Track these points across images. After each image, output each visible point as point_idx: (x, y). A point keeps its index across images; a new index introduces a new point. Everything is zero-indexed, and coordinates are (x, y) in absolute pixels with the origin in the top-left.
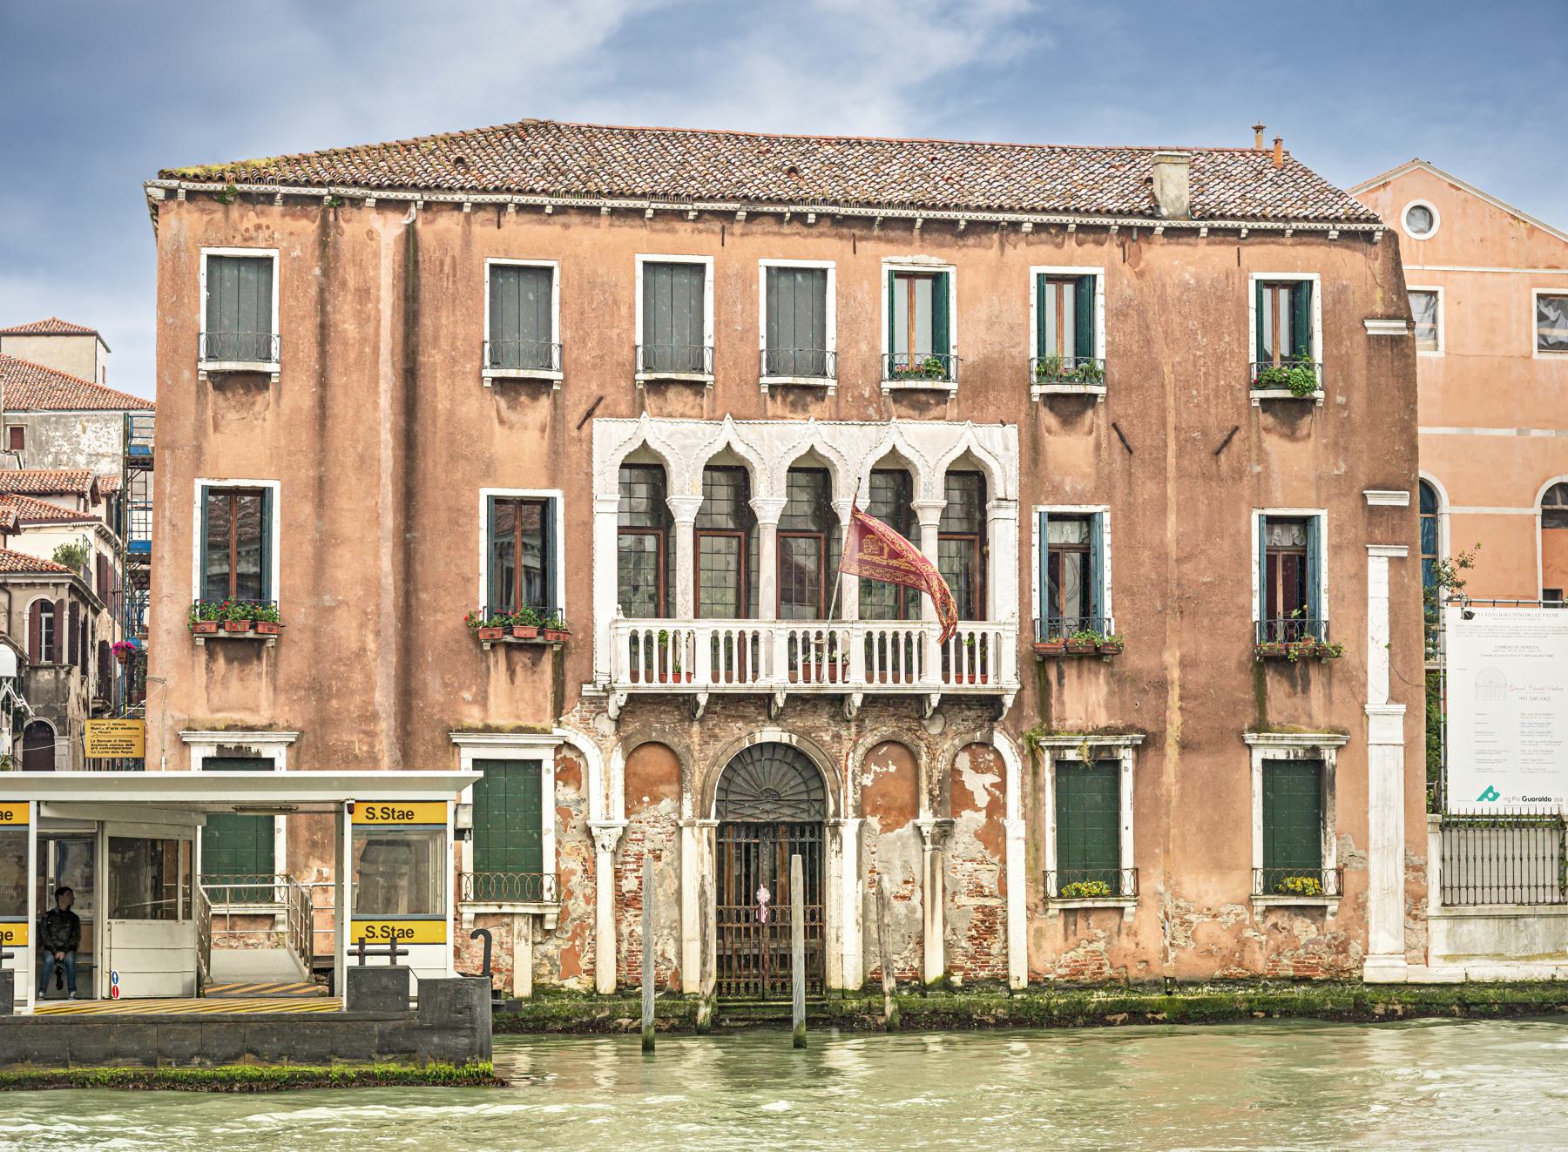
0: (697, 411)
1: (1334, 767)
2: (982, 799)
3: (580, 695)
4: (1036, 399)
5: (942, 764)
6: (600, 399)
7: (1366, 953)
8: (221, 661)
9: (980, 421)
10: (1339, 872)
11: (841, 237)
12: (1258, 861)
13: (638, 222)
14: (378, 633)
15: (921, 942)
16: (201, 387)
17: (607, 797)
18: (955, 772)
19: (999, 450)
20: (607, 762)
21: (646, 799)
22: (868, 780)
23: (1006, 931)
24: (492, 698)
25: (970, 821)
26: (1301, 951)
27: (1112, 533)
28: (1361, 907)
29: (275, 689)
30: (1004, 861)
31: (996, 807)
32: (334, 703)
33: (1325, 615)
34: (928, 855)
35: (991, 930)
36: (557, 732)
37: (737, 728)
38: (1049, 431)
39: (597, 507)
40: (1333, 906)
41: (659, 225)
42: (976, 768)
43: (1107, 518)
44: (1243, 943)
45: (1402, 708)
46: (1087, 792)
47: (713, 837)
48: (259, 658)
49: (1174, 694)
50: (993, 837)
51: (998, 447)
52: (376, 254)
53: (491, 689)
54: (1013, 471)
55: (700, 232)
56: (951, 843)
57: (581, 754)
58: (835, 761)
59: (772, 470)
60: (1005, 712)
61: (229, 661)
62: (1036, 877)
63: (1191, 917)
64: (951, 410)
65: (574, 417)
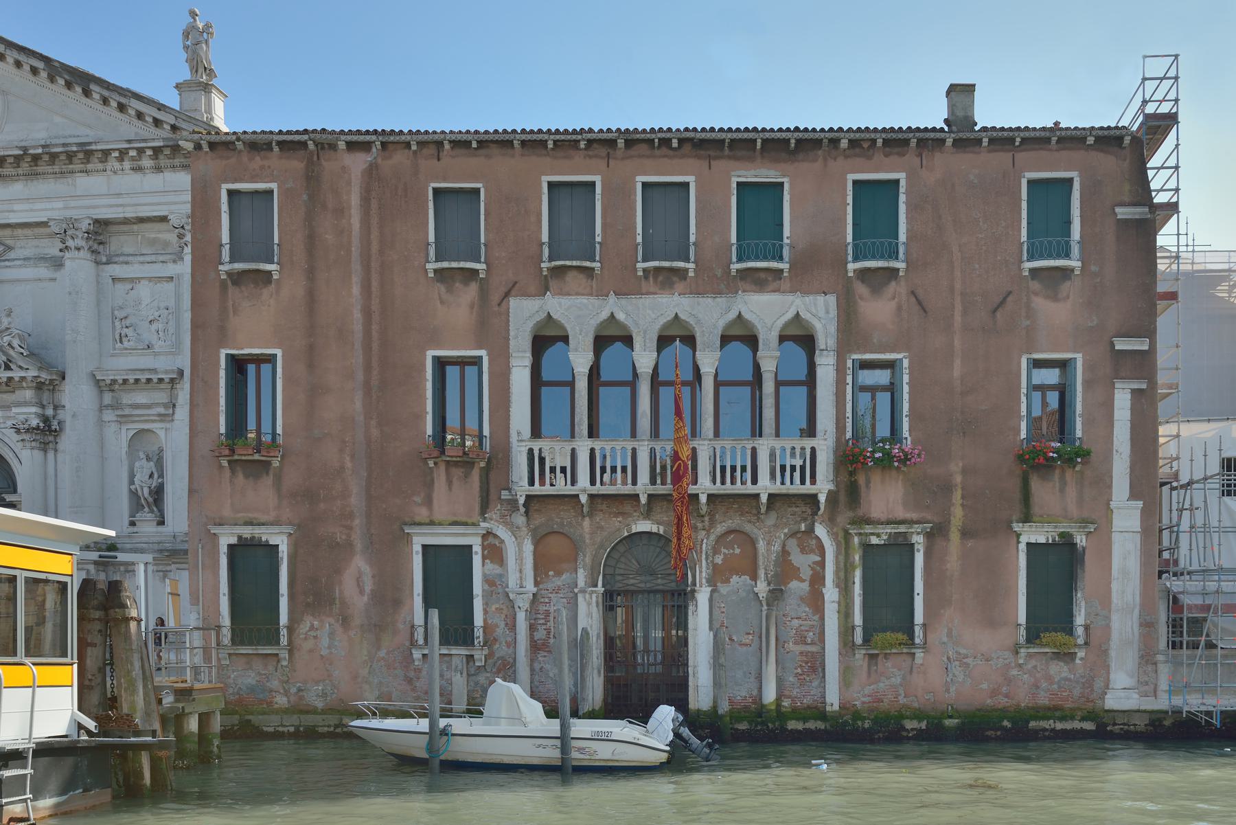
1: (1084, 549)
2: (806, 573)
3: (500, 498)
4: (851, 274)
5: (777, 547)
7: (1107, 687)
8: (240, 476)
9: (806, 293)
10: (1087, 628)
11: (699, 157)
12: (1022, 618)
13: (544, 152)
14: (353, 457)
17: (521, 571)
18: (785, 552)
20: (520, 546)
21: (551, 573)
22: (719, 560)
24: (435, 502)
25: (798, 587)
26: (1055, 686)
27: (910, 374)
28: (1104, 653)
30: (822, 619)
31: (817, 580)
32: (322, 506)
33: (1079, 434)
34: (764, 613)
36: (483, 524)
37: (616, 522)
38: (861, 298)
39: (513, 362)
40: (1081, 654)
42: (804, 550)
43: (906, 363)
44: (1009, 681)
45: (1140, 504)
47: (600, 600)
48: (267, 473)
49: (957, 496)
50: (816, 600)
51: (820, 312)
52: (349, 183)
53: (435, 495)
54: (833, 328)
55: (590, 157)
57: (502, 542)
59: (645, 332)
60: (822, 507)
61: (246, 477)
62: (846, 631)
63: (969, 661)
64: (786, 285)
65: (495, 297)
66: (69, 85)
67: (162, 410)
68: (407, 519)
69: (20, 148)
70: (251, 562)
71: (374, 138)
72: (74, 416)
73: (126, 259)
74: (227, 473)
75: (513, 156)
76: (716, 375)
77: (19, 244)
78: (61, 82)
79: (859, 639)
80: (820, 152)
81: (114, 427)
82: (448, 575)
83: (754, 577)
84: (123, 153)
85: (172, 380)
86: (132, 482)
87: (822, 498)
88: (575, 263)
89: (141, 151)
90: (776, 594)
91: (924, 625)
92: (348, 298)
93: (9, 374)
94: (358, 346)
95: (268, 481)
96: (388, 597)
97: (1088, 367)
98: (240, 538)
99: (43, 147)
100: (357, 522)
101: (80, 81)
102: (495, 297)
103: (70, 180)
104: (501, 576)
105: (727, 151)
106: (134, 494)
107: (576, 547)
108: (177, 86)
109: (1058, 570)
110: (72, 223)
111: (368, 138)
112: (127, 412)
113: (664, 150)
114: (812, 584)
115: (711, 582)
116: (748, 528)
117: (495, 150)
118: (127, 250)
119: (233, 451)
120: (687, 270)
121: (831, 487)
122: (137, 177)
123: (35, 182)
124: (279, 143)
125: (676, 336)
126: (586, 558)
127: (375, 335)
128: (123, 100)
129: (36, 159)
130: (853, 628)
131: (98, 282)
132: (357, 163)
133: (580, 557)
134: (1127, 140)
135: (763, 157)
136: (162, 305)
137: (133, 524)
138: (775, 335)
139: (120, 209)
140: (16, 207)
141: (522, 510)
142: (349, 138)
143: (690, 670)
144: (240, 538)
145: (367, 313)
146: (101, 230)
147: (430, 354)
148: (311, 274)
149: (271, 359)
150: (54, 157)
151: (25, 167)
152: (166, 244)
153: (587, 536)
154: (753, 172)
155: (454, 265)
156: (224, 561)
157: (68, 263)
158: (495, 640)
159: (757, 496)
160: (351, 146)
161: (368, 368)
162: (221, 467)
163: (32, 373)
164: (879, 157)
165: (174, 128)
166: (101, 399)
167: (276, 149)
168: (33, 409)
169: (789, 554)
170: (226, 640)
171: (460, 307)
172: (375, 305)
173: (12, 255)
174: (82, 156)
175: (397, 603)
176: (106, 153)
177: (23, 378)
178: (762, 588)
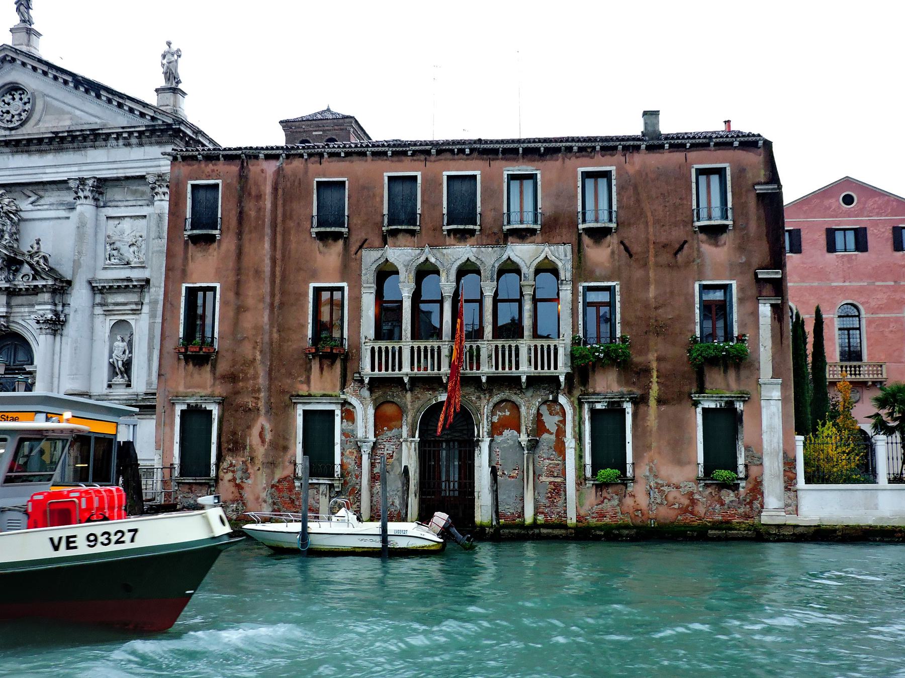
0: (412, 244)
1: (742, 411)
2: (553, 429)
5: (533, 411)
6: (366, 240)
7: (762, 507)
8: (191, 365)
9: (550, 243)
10: (746, 466)
12: (701, 460)
14: (261, 352)
15: (522, 499)
16: (186, 243)
18: (539, 415)
19: (562, 257)
20: (365, 410)
22: (495, 419)
23: (565, 495)
24: (312, 381)
25: (547, 439)
27: (621, 295)
29: (215, 379)
30: (564, 459)
35: (558, 494)
36: (342, 396)
37: (428, 394)
40: (743, 484)
41: (395, 158)
43: (618, 288)
44: (693, 502)
45: (780, 381)
46: (607, 425)
50: (560, 448)
53: (312, 377)
56: (537, 451)
57: (354, 407)
58: (478, 410)
60: (563, 385)
61: (194, 365)
62: (581, 467)
63: (665, 488)
64: (538, 238)
65: (353, 249)
66: (87, 91)
67: (134, 307)
68: (294, 393)
69: (53, 133)
70: (195, 419)
71: (281, 152)
72: (76, 311)
73: (116, 204)
74: (183, 363)
75: (366, 161)
76: (496, 294)
77: (47, 194)
78: (82, 89)
79: (589, 473)
80: (560, 155)
81: (101, 318)
82: (319, 426)
83: (519, 432)
84: (119, 135)
85: (142, 286)
86: (111, 357)
87: (562, 379)
88: (404, 227)
89: (130, 133)
90: (534, 445)
91: (633, 464)
92: (262, 251)
93: (35, 283)
94: (267, 281)
95: (208, 368)
96: (280, 445)
97: (741, 289)
98: (188, 405)
99: (68, 132)
100: (262, 394)
101: (93, 88)
102: (353, 249)
103: (83, 152)
104: (353, 431)
105: (500, 156)
106: (112, 365)
107: (402, 411)
108: (157, 90)
109: (725, 427)
110: (82, 181)
111: (278, 152)
112: (110, 308)
113: (461, 156)
114: (557, 436)
115: (491, 434)
116: (514, 398)
117: (355, 158)
118: (118, 197)
119: (186, 350)
120: (475, 230)
121: (569, 370)
122: (127, 149)
123: (61, 154)
124: (223, 156)
125: (467, 269)
126: (408, 419)
127: (278, 274)
128: (121, 101)
129: (63, 139)
130: (585, 466)
131: (97, 219)
132: (271, 167)
133: (404, 419)
134: (761, 143)
135: (523, 158)
136: (138, 235)
137: (110, 386)
138: (532, 270)
139: (115, 171)
140: (48, 170)
141: (367, 387)
142: (266, 152)
143: (476, 494)
144: (188, 405)
145: (274, 261)
146: (102, 186)
147: (312, 285)
148: (240, 234)
149: (213, 289)
150: (74, 138)
151: (55, 145)
152: (143, 193)
153: (409, 404)
154: (517, 168)
155: (328, 229)
156: (178, 421)
157: (78, 208)
158: (348, 473)
159: (519, 378)
160: (268, 157)
161: (273, 295)
162: (179, 359)
163: (50, 282)
164: (598, 157)
165: (153, 119)
166: (94, 299)
167: (222, 159)
168: (49, 307)
169: (542, 415)
170: (176, 473)
171: (333, 254)
172: (279, 255)
173: (42, 202)
174: (93, 138)
175: (285, 449)
176: (108, 135)
177: (44, 286)
178: (524, 438)
